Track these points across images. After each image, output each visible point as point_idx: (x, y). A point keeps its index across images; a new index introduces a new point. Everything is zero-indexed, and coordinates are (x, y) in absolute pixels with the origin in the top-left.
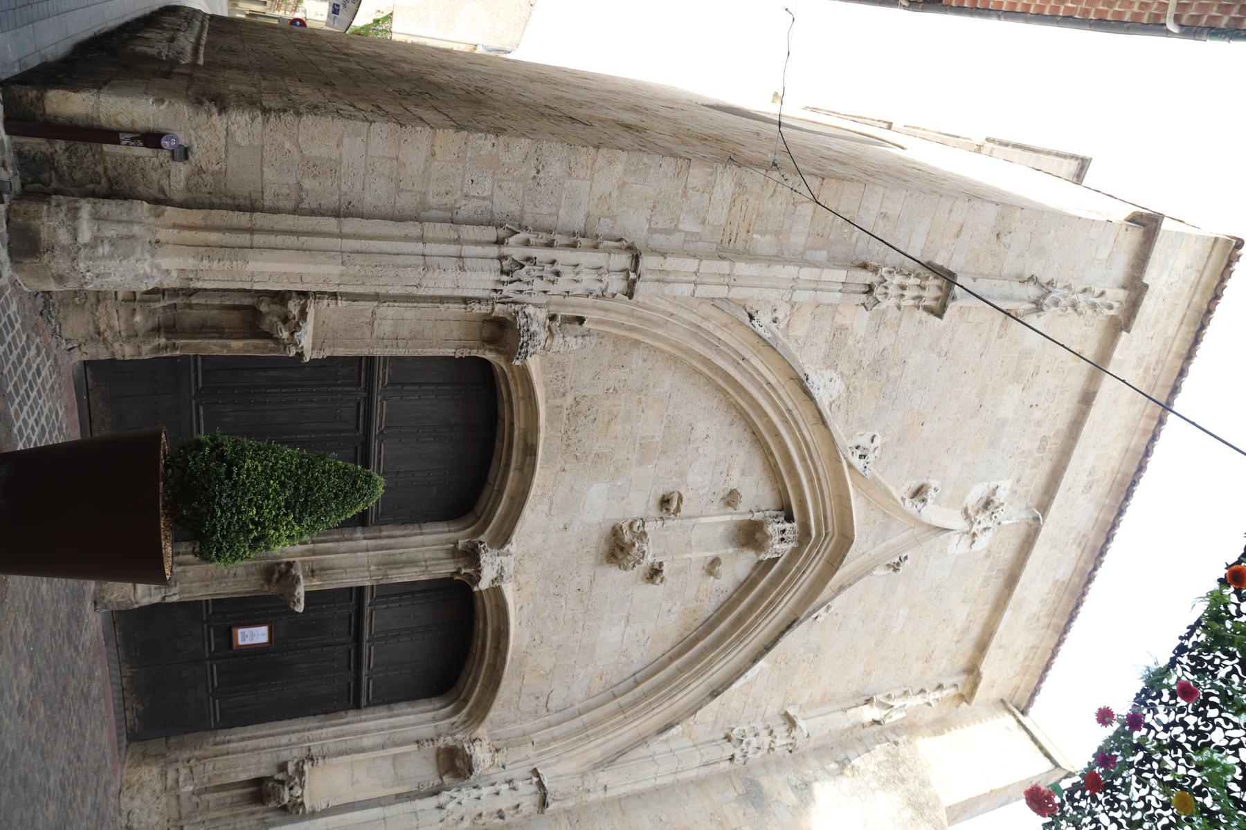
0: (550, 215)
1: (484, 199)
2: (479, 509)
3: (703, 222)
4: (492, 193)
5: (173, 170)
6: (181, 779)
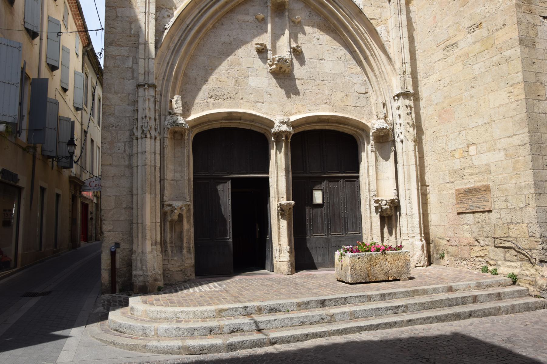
0: (129, 119)
1: (125, 145)
2: (263, 132)
3: (128, 57)
4: (123, 142)
5: (123, 248)
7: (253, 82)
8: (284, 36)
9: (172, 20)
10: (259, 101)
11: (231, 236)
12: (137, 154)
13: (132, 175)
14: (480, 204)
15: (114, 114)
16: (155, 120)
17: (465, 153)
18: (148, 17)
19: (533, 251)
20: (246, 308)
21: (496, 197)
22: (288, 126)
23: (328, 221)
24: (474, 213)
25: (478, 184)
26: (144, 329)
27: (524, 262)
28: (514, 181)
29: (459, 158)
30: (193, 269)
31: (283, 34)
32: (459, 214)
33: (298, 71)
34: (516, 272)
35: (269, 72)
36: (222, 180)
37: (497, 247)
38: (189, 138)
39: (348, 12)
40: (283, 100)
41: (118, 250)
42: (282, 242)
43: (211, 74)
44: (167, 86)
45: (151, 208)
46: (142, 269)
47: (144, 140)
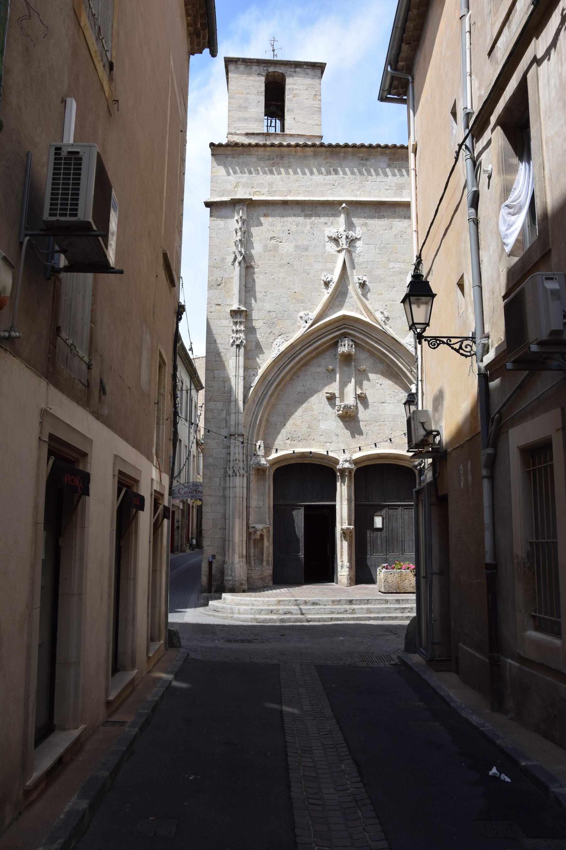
1: (220, 480)
2: (331, 467)
3: (222, 410)
7: (323, 425)
9: (257, 379)
10: (328, 441)
11: (303, 553)
12: (229, 487)
13: (225, 504)
15: (212, 456)
16: (243, 461)
18: (238, 379)
20: (296, 600)
22: (350, 463)
23: (386, 543)
30: (270, 578)
31: (350, 382)
33: (362, 414)
36: (296, 507)
38: (270, 474)
40: (348, 440)
41: (214, 560)
42: (344, 560)
43: (288, 420)
44: (253, 433)
45: (239, 529)
46: (231, 576)
47: (234, 477)
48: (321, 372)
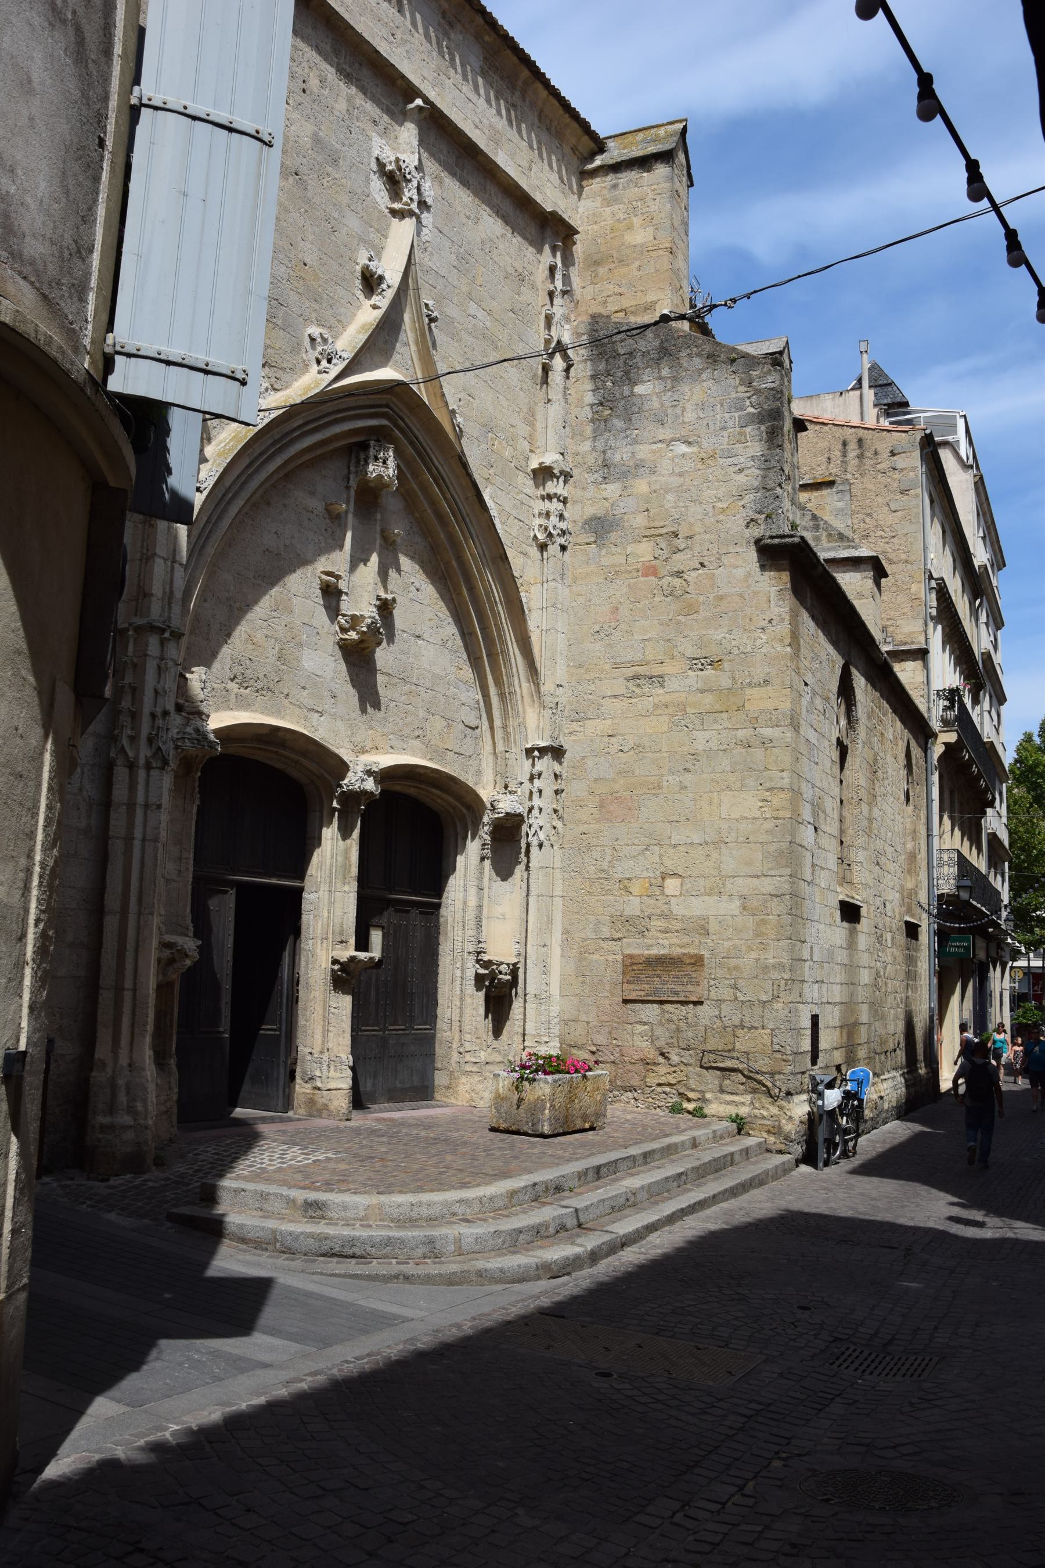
6: (475, 1060)
8: (365, 565)
10: (316, 708)
11: (228, 1026)
14: (679, 988)
17: (656, 889)
19: (777, 1077)
21: (714, 979)
24: (662, 1002)
25: (677, 951)
26: (430, 1242)
27: (757, 1096)
28: (754, 955)
29: (640, 896)
32: (626, 1001)
34: (744, 1111)
35: (338, 643)
37: (707, 1068)
39: (480, 551)
43: (237, 623)
46: (131, 1110)
48: (315, 512)
